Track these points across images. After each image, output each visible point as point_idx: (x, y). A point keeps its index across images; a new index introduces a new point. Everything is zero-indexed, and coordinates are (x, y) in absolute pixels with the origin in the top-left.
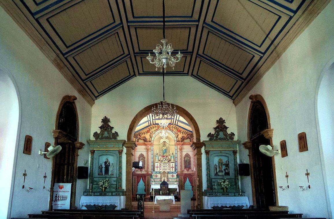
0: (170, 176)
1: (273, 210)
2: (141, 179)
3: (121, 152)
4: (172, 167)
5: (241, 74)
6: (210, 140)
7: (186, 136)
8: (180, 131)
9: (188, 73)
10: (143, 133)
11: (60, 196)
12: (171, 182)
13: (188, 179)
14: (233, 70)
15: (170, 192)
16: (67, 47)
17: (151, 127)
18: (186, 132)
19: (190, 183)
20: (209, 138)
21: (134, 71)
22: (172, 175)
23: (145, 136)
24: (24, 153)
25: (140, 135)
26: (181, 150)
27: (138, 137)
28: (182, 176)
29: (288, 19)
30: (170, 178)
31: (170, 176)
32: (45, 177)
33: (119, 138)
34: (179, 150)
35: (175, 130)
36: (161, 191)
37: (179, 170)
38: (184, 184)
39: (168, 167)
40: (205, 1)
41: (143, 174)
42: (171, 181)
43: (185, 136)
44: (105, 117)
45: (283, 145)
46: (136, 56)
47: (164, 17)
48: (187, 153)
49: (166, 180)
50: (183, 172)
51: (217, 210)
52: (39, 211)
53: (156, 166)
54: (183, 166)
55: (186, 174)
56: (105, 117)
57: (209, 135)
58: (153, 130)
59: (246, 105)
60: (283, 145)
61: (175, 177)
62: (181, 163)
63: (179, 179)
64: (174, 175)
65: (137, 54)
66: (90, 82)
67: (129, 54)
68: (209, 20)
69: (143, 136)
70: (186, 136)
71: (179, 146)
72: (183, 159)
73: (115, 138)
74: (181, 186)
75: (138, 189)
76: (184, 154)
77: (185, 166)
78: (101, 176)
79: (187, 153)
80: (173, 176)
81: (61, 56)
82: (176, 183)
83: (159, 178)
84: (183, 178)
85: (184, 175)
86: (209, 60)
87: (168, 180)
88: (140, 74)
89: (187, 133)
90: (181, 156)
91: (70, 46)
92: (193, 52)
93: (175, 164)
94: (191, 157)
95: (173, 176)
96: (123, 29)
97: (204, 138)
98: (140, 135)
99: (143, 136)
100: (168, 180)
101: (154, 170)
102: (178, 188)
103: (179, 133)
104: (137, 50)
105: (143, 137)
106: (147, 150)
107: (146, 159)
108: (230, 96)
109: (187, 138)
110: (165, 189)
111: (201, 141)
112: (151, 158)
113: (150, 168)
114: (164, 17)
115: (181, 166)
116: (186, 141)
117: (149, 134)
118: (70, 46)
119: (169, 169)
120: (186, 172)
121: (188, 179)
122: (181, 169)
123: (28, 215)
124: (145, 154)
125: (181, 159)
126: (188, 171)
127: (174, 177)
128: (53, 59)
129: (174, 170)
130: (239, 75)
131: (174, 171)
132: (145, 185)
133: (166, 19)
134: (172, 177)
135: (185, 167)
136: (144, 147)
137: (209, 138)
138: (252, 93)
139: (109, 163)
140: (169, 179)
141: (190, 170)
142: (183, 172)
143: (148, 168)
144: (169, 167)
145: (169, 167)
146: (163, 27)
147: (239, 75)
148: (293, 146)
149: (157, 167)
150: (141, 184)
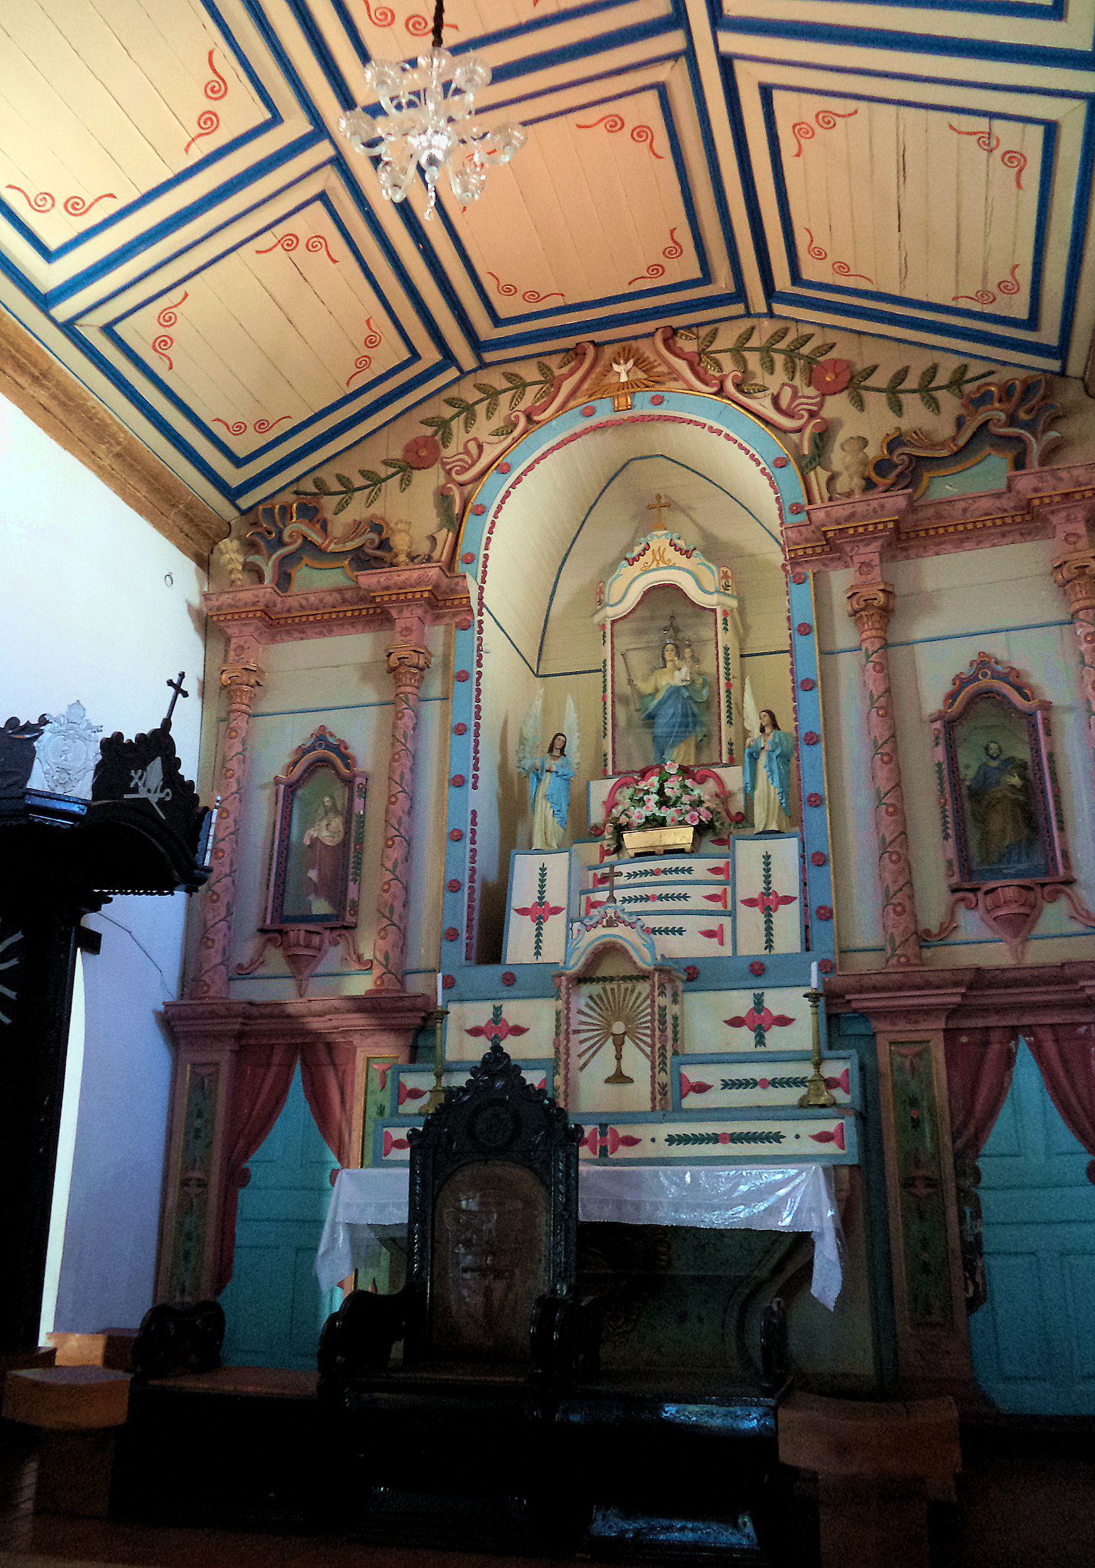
0: (707, 1020)
1: (251, 1389)
2: (290, 1067)
4: (768, 903)
7: (941, 426)
8: (854, 383)
10: (359, 481)
13: (1027, 1075)
18: (943, 377)
19: (1067, 1139)
22: (741, 1002)
23: (377, 509)
25: (309, 512)
26: (882, 613)
27: (296, 527)
28: (927, 1012)
31: (707, 1020)
34: (845, 634)
35: (776, 381)
37: (865, 923)
38: (975, 1144)
39: (697, 897)
43: (938, 423)
48: (983, 663)
51: (12, 989)
53: (522, 893)
54: (933, 856)
55: (980, 979)
58: (483, 427)
61: (802, 1031)
62: (894, 802)
63: (868, 1074)
64: (777, 1001)
69: (357, 510)
70: (941, 426)
71: (841, 580)
72: (923, 757)
74: (908, 1183)
75: (243, 1234)
76: (934, 674)
79: (983, 663)
80: (760, 1021)
82: (800, 1135)
84: (938, 1052)
89: (957, 382)
90: (888, 703)
93: (802, 842)
94: (1047, 707)
95: (760, 1021)
98: (309, 512)
99: (357, 510)
101: (489, 944)
102: (823, 1220)
103: (837, 406)
106: (400, 675)
107: (374, 809)
112: (441, 772)
113: (435, 910)
115: (897, 849)
117: (428, 481)
119: (712, 923)
120: (980, 943)
121: (1027, 1075)
122: (901, 895)
124: (362, 736)
125: (889, 750)
126: (1020, 924)
127: (776, 1038)
129: (788, 938)
134: (744, 1039)
135: (967, 883)
136: (357, 646)
140: (693, 1074)
141: (1054, 916)
143: (398, 926)
144: (730, 908)
145: (717, 906)
149: (540, 912)
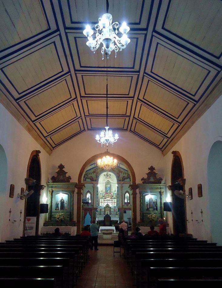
3: (73, 192)
5: (167, 134)
6: (143, 183)
9: (127, 129)
11: (28, 227)
12: (113, 215)
14: (160, 131)
15: (111, 223)
16: (19, 94)
17: (97, 168)
20: (150, 171)
21: (84, 127)
23: (91, 176)
24: (10, 197)
25: (87, 175)
29: (136, 181)
30: (112, 212)
32: (21, 213)
33: (71, 181)
36: (74, 252)
40: (155, 2)
41: (90, 208)
42: (113, 214)
44: (61, 164)
45: (191, 190)
46: (68, 34)
47: (107, 94)
49: (109, 214)
50: (123, 207)
52: (51, 233)
56: (61, 164)
57: (143, 179)
59: (170, 158)
60: (191, 190)
65: (84, 98)
66: (50, 137)
67: (81, 116)
68: (136, 116)
73: (69, 181)
77: (198, 118)
78: (58, 211)
81: (31, 122)
82: (117, 216)
83: (103, 212)
85: (124, 209)
86: (141, 122)
87: (110, 214)
88: (88, 129)
91: (21, 93)
92: (130, 116)
96: (71, 77)
97: (138, 181)
100: (110, 214)
104: (87, 114)
105: (90, 177)
108: (160, 148)
109: (127, 178)
110: (108, 221)
111: (137, 184)
114: (107, 94)
116: (126, 180)
118: (49, 133)
123: (5, 241)
128: (25, 126)
130: (165, 135)
131: (116, 206)
132: (91, 218)
133: (108, 96)
137: (150, 171)
138: (174, 149)
139: (64, 201)
140: (112, 213)
142: (123, 207)
146: (106, 100)
147: (165, 135)
148: (195, 191)
150: (88, 217)
